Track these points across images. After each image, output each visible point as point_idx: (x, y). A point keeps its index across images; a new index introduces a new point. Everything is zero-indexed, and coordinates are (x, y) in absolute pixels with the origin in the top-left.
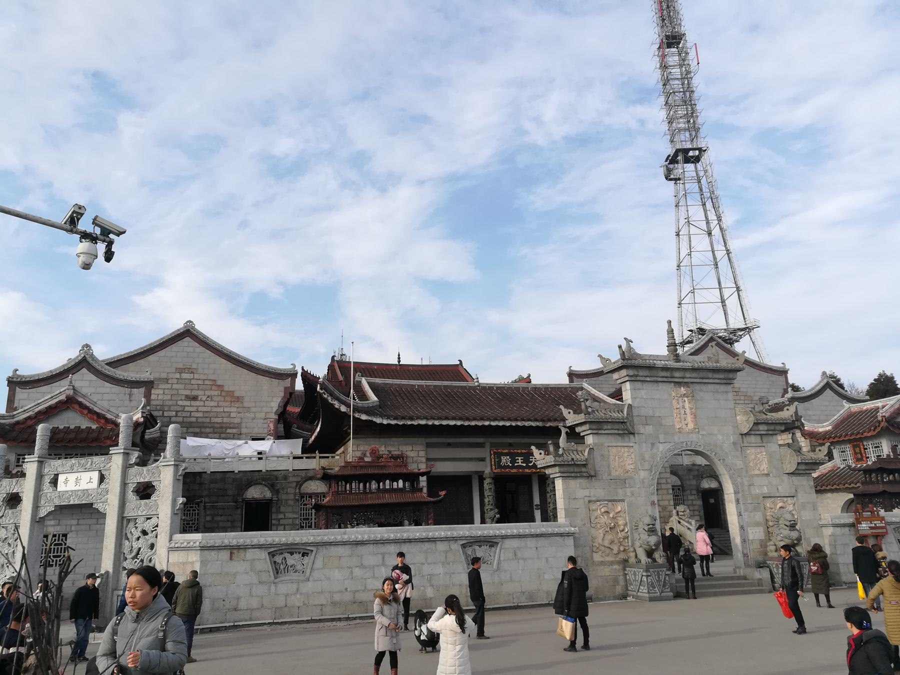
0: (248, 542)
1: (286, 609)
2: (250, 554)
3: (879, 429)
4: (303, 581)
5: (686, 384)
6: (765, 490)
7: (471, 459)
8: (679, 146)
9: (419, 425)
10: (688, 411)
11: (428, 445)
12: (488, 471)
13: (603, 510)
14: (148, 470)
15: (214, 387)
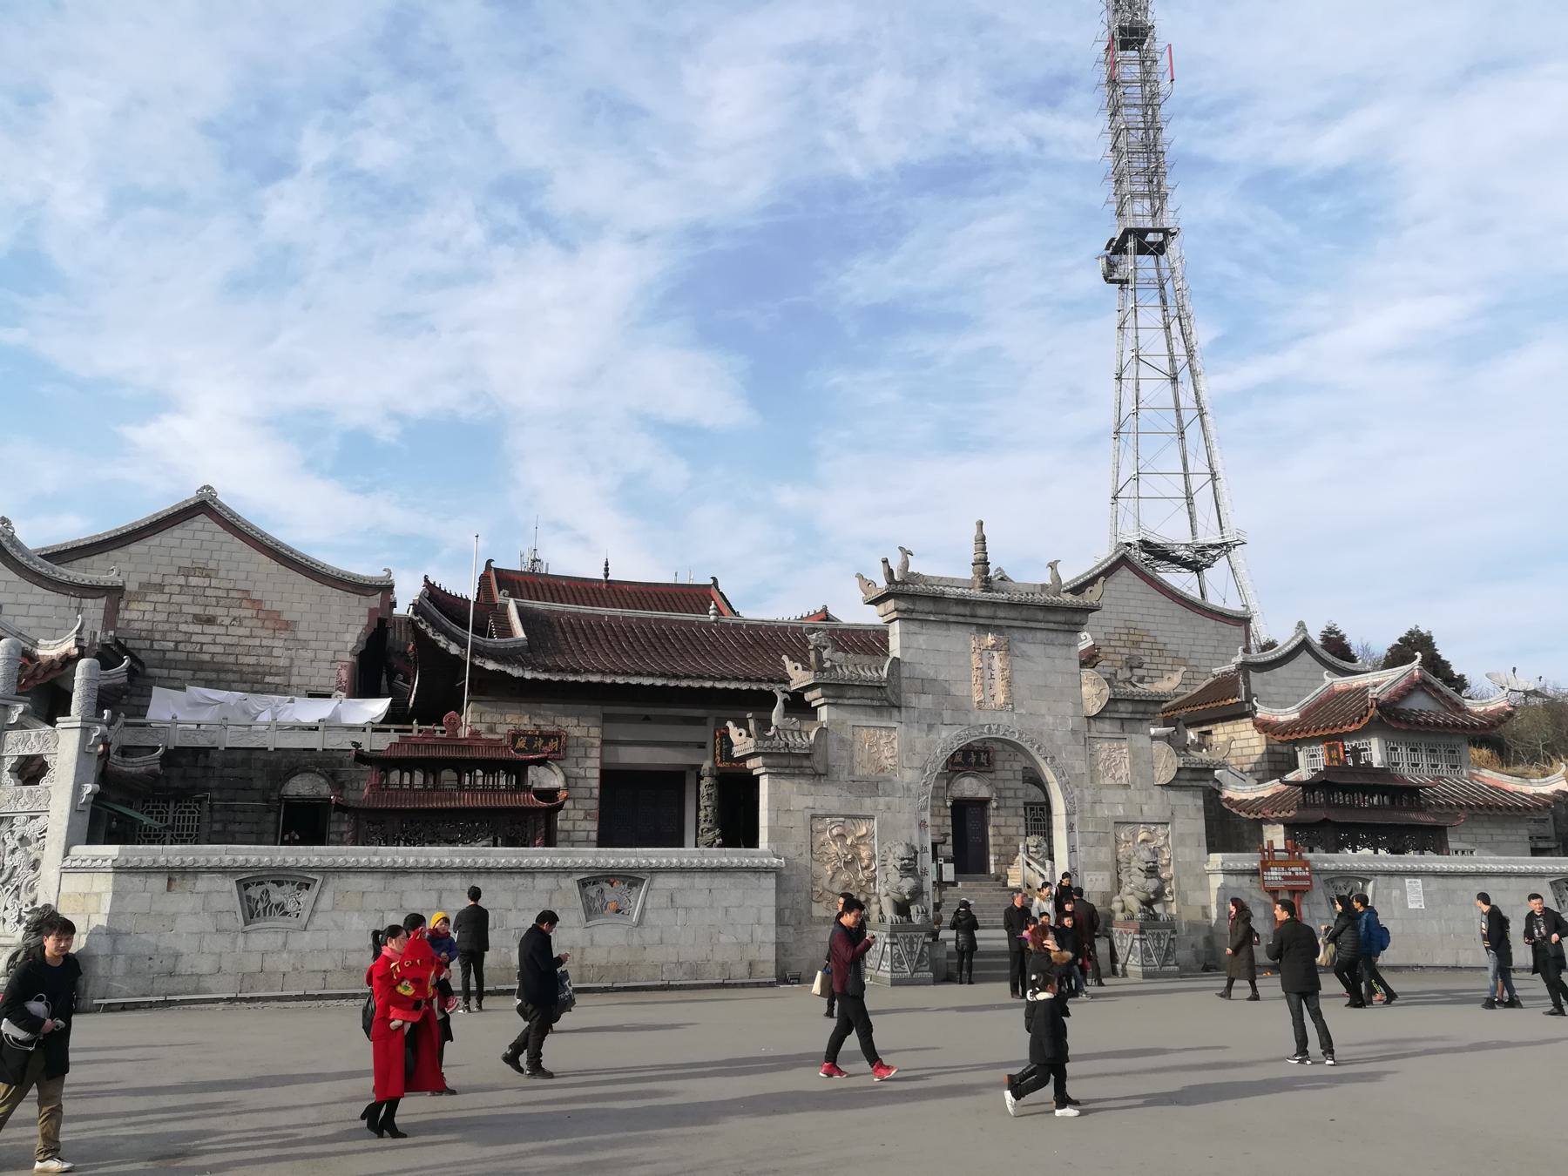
0: (202, 861)
1: (262, 976)
2: (203, 883)
3: (1366, 720)
4: (294, 930)
5: (997, 629)
7: (685, 744)
8: (1130, 224)
9: (589, 683)
10: (997, 674)
11: (607, 719)
12: (707, 765)
13: (835, 832)
14: (38, 736)
15: (245, 603)
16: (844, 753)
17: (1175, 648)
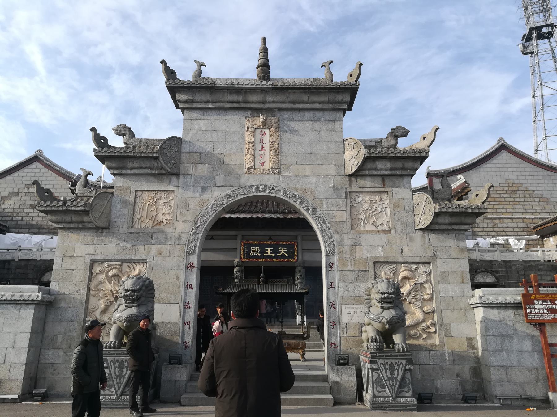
5: (270, 111)
6: (380, 253)
8: (533, 26)
10: (267, 146)
13: (110, 273)
16: (126, 212)
17: (540, 192)
